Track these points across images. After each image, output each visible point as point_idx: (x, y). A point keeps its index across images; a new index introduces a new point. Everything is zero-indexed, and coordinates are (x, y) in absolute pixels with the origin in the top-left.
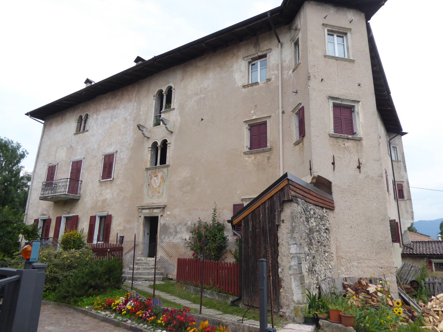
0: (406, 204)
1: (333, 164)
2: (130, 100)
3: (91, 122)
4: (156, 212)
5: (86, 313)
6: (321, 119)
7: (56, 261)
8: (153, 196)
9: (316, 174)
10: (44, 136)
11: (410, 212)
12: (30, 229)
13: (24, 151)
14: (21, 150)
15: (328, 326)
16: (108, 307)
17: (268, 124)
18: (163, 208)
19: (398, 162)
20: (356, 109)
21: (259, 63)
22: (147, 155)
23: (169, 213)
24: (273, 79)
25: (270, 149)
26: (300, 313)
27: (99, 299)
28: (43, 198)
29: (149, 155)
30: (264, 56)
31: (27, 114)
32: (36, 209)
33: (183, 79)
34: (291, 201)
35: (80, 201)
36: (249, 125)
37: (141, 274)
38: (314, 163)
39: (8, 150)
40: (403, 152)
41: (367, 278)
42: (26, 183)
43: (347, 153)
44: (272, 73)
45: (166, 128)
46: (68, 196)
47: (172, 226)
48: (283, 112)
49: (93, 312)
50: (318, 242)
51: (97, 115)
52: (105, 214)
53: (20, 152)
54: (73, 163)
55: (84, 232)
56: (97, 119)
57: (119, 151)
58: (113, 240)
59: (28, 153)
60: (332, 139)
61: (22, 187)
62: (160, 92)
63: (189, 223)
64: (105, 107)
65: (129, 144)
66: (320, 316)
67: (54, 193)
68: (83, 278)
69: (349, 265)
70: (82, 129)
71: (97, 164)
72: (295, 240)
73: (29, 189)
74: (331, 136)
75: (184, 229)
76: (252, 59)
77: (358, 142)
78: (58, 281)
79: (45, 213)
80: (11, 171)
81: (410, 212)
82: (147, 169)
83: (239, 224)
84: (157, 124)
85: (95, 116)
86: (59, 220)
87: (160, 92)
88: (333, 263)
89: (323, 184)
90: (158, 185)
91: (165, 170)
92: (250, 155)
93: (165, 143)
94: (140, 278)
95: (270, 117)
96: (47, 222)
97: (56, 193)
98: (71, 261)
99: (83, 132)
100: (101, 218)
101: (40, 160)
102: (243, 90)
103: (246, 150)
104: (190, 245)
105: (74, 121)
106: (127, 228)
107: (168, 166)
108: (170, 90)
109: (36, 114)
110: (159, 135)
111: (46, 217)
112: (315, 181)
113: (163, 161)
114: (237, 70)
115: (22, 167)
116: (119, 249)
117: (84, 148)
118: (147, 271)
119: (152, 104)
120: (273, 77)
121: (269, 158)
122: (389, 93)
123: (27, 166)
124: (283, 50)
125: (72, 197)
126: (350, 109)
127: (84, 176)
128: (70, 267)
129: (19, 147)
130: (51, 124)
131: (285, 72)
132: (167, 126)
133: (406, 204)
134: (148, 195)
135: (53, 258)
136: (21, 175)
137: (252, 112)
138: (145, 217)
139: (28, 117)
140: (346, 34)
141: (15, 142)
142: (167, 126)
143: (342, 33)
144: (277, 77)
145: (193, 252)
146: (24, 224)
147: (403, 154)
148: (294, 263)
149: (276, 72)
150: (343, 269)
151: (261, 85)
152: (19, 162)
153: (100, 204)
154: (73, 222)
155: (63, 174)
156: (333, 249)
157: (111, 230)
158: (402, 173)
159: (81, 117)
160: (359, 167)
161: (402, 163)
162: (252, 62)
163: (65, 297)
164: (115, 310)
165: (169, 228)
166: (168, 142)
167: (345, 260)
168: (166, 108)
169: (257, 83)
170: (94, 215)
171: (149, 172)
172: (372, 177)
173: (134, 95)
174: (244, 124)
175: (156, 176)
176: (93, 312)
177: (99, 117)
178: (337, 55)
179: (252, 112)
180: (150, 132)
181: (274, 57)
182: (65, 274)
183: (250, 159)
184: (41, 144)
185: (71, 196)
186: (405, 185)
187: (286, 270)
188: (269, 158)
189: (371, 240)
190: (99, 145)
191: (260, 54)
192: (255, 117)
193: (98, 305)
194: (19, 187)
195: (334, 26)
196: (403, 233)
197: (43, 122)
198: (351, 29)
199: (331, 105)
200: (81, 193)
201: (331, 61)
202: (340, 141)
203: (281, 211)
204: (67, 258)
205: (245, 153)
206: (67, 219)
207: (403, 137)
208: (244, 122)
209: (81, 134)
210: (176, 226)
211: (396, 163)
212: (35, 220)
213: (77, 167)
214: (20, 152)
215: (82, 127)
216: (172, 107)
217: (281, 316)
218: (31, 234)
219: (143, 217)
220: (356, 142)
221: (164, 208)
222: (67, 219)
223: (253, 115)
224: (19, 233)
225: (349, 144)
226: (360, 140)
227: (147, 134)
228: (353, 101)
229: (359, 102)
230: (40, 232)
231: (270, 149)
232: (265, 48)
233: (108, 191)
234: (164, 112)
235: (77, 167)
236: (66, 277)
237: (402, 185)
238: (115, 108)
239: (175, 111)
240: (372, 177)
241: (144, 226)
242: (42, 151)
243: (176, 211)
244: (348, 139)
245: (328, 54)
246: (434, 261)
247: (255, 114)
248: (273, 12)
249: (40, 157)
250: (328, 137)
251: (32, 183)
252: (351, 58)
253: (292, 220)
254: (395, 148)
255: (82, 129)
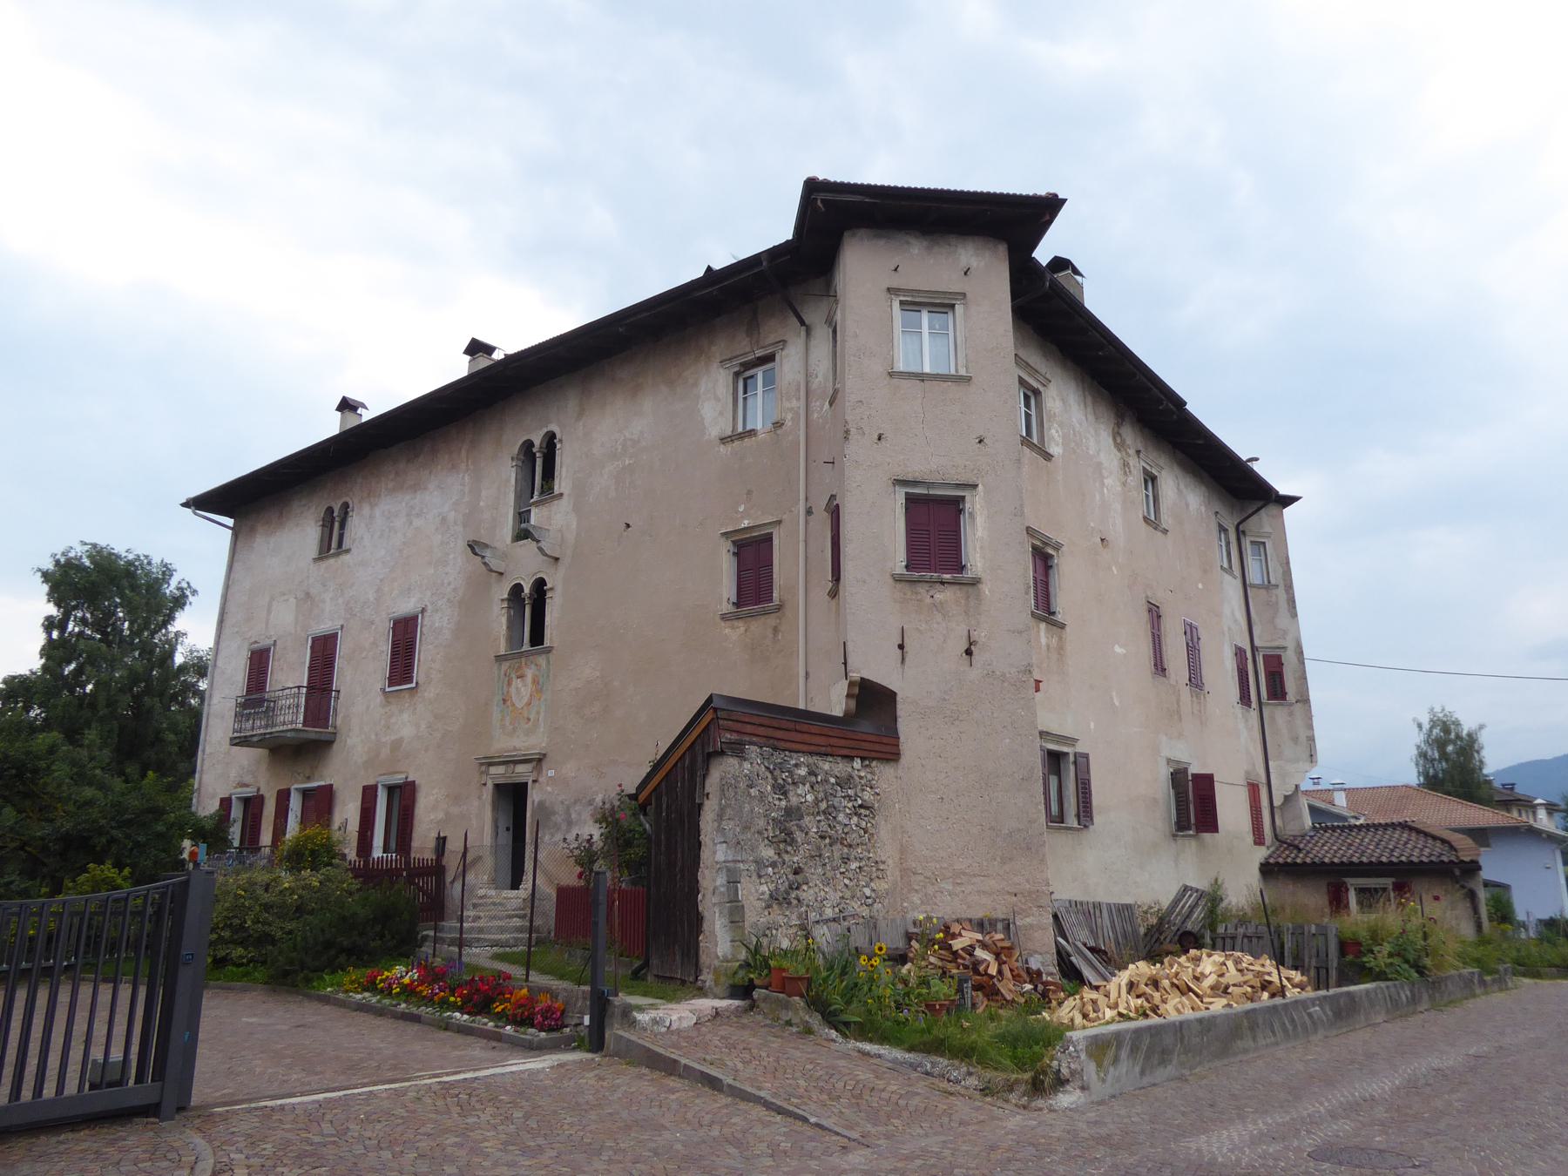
0: (1291, 714)
1: (901, 647)
2: (454, 467)
3: (357, 527)
4: (522, 772)
5: (326, 1000)
6: (880, 534)
7: (266, 898)
8: (514, 730)
9: (855, 676)
10: (236, 565)
11: (1303, 738)
12: (209, 825)
13: (184, 585)
14: (174, 583)
15: (765, 1000)
16: (370, 986)
17: (776, 542)
18: (539, 761)
19: (1271, 592)
20: (967, 505)
21: (759, 373)
22: (498, 618)
23: (551, 773)
24: (788, 423)
25: (779, 608)
26: (723, 979)
27: (355, 974)
28: (240, 741)
29: (504, 620)
30: (770, 358)
31: (186, 505)
32: (223, 771)
33: (581, 414)
34: (722, 753)
35: (335, 746)
36: (734, 542)
37: (481, 930)
38: (850, 647)
39: (134, 588)
40: (1287, 558)
41: (970, 921)
42: (194, 685)
43: (939, 617)
44: (787, 405)
45: (540, 549)
46: (305, 735)
47: (560, 809)
48: (809, 512)
49: (341, 996)
50: (823, 837)
51: (372, 506)
52: (398, 779)
53: (171, 589)
54: (314, 640)
55: (349, 828)
56: (372, 517)
57: (430, 608)
58: (422, 843)
59: (194, 592)
60: (899, 585)
61: (185, 698)
62: (528, 445)
63: (599, 799)
64: (391, 485)
65: (455, 590)
66: (757, 982)
67: (267, 726)
68: (323, 930)
69: (930, 890)
70: (334, 544)
71: (374, 644)
72: (724, 835)
73: (202, 700)
74: (898, 579)
75: (587, 814)
76: (741, 364)
77: (970, 589)
78: (273, 942)
79: (248, 779)
80: (147, 649)
81: (1303, 738)
82: (499, 659)
83: (647, 802)
84: (523, 535)
85: (366, 510)
86: (283, 797)
87: (528, 445)
88: (881, 886)
89: (873, 700)
90: (526, 700)
91: (542, 660)
92: (736, 623)
93: (540, 585)
94: (479, 940)
95: (779, 522)
96: (253, 805)
97: (273, 725)
98: (300, 897)
99: (337, 555)
100: (391, 789)
101: (227, 631)
102: (723, 449)
103: (727, 608)
104: (577, 852)
105: (312, 523)
106: (453, 815)
107: (549, 650)
108: (551, 439)
109: (207, 503)
110: (525, 566)
111: (249, 792)
112: (856, 690)
113: (537, 637)
114: (706, 395)
115: (178, 634)
116: (436, 870)
117: (340, 601)
118: (499, 923)
119: (508, 481)
120: (789, 416)
121: (776, 630)
122: (1180, 403)
123: (194, 631)
124: (813, 343)
125: (313, 736)
126: (954, 506)
127: (345, 676)
128: (300, 910)
129: (167, 572)
130: (252, 530)
131: (815, 405)
132: (542, 544)
133: (1291, 714)
134: (503, 727)
135: (260, 891)
136: (179, 659)
137: (741, 509)
138: (497, 786)
139: (188, 511)
140: (952, 306)
141: (156, 560)
142: (542, 544)
143: (942, 304)
144: (796, 419)
145: (578, 869)
146: (193, 814)
147: (1288, 563)
148: (721, 880)
149: (794, 403)
150: (916, 899)
151: (761, 436)
152: (170, 618)
153: (385, 752)
154: (320, 802)
155: (290, 675)
156: (887, 850)
157: (416, 822)
158: (1283, 621)
159: (330, 510)
160: (969, 652)
161: (1281, 593)
162: (744, 373)
163: (286, 974)
164: (382, 991)
165: (554, 813)
166: (549, 586)
167: (921, 878)
168: (542, 493)
169: (752, 433)
170: (371, 782)
171: (505, 666)
172: (1003, 675)
173: (464, 453)
174: (723, 540)
175: (521, 677)
176: (341, 996)
177: (377, 512)
178: (927, 369)
179: (741, 509)
180: (504, 556)
181: (789, 365)
182: (289, 926)
183: (734, 633)
184: (227, 587)
185: (313, 732)
186: (1289, 659)
187: (709, 896)
188: (776, 630)
189: (992, 828)
190: (378, 591)
191: (759, 353)
192: (746, 523)
193: (352, 982)
194: (174, 698)
195: (919, 291)
196: (1277, 802)
197: (230, 522)
198: (964, 295)
199: (901, 500)
200: (339, 722)
201: (905, 384)
202: (922, 589)
203: (704, 777)
204: (292, 891)
205: (724, 617)
206: (306, 794)
207: (1288, 512)
208: (724, 534)
209: (332, 561)
210: (568, 809)
211: (1263, 592)
212: (222, 800)
213: (324, 651)
214: (171, 589)
215: (332, 542)
216: (557, 491)
217: (701, 989)
218: (212, 835)
219: (490, 785)
220: (965, 588)
221: (540, 760)
222: (306, 794)
223: (743, 518)
224: (182, 838)
225: (945, 595)
226: (975, 582)
227: (495, 564)
228: (958, 486)
229: (975, 486)
230: (235, 833)
231: (779, 608)
232: (772, 338)
233: (405, 716)
234: (537, 504)
235: (324, 651)
236: (290, 932)
237: (1279, 657)
238: (416, 488)
239: (564, 502)
240: (1003, 675)
241: (495, 808)
242: (231, 607)
243: (569, 769)
244: (943, 583)
245: (901, 366)
246: (1353, 882)
247: (745, 515)
248: (775, 253)
249: (227, 624)
250: (891, 581)
251: (211, 685)
252: (962, 372)
253: (735, 788)
254: (1260, 545)
255: (334, 544)
